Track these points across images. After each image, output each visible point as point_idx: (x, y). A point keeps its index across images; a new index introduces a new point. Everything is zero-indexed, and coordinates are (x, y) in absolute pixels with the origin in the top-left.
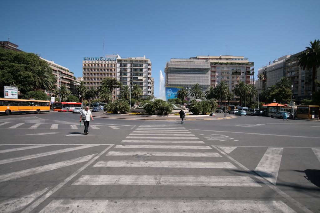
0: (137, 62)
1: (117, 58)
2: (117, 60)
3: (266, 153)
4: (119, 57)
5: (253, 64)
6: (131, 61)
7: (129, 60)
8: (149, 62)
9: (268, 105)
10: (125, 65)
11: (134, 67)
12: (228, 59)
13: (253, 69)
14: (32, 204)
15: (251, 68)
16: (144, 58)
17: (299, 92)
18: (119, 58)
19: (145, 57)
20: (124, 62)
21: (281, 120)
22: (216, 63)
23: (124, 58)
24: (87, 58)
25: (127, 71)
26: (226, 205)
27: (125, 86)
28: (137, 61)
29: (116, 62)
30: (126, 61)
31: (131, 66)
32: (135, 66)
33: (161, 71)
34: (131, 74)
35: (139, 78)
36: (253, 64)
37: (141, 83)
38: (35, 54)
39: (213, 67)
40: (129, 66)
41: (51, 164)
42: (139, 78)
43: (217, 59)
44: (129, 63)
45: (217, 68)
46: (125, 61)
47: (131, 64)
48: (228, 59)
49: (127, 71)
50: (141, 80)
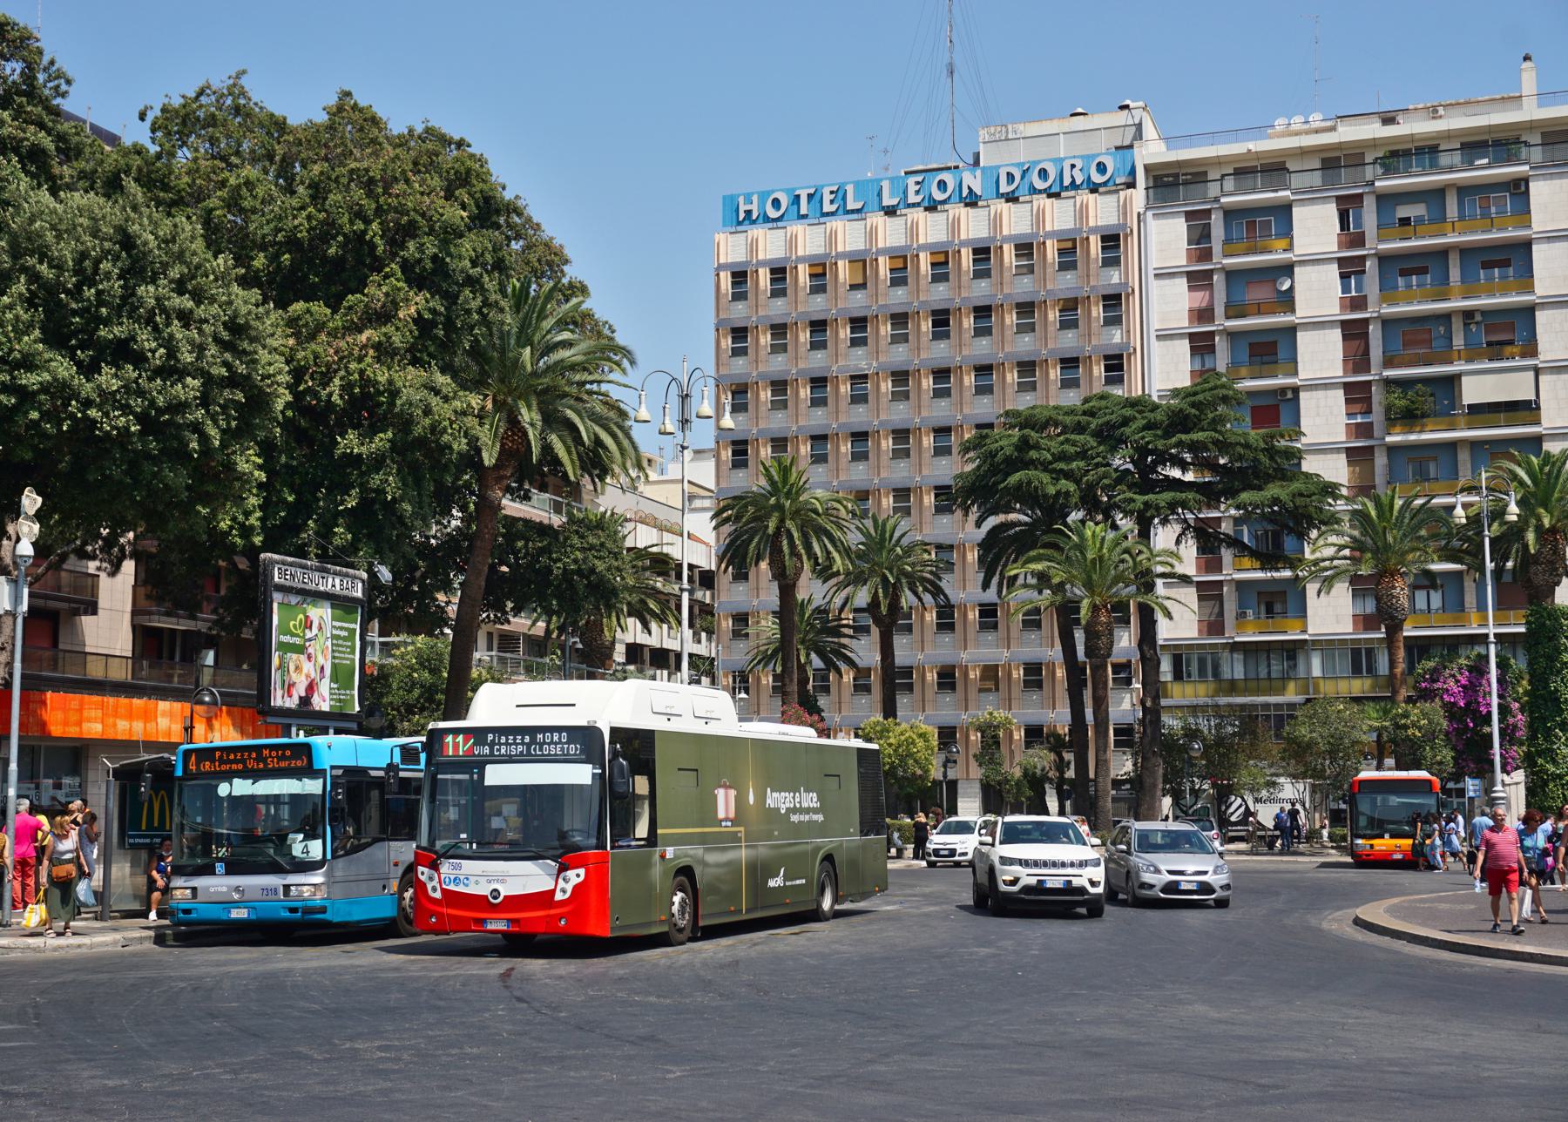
0: (1434, 167)
6: (1334, 161)
7: (1303, 152)
11: (1388, 363)
14: (1389, 651)
17: (63, 574)
21: (941, 540)
23: (1235, 134)
25: (1287, 301)
26: (935, 166)
29: (1138, 197)
30: (1273, 169)
31: (1352, 237)
32: (1410, 417)
34: (1354, 333)
38: (557, 242)
44: (1312, 196)
46: (1246, 171)
47: (1347, 208)
49: (1291, 308)
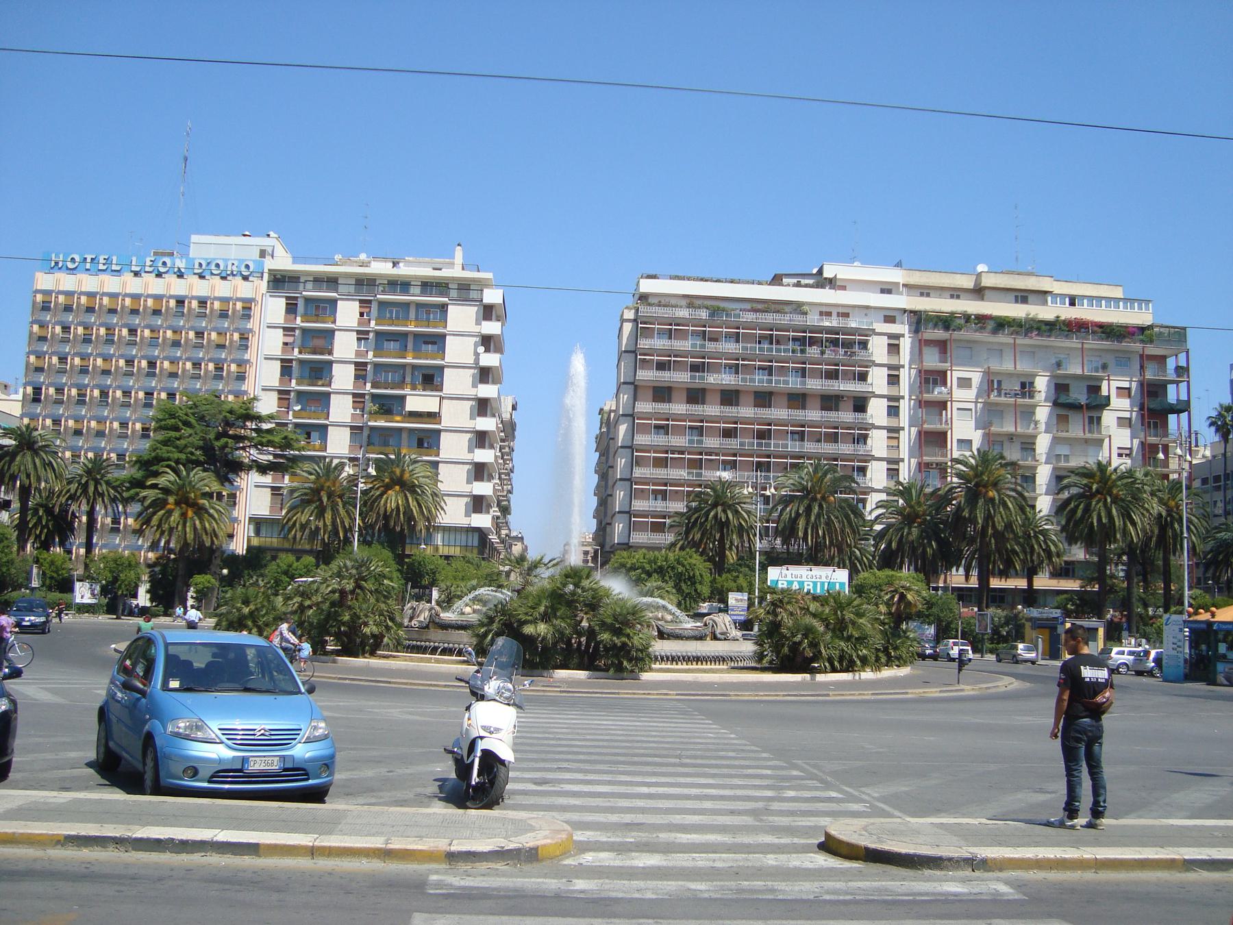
1: (269, 264)
2: (266, 276)
3: (14, 772)
4: (280, 251)
5: (1178, 336)
6: (365, 283)
7: (347, 275)
8: (492, 296)
9: (1213, 615)
10: (326, 308)
12: (1022, 296)
13: (1182, 371)
15: (1171, 363)
16: (455, 271)
18: (283, 261)
19: (459, 254)
20: (423, 293)
22: (946, 322)
24: (241, 261)
27: (1185, 535)
28: (402, 285)
30: (331, 281)
33: (578, 364)
35: (417, 401)
36: (1178, 336)
37: (427, 440)
39: (929, 343)
40: (348, 313)
41: (1020, 921)
42: (417, 401)
43: (955, 293)
45: (953, 350)
48: (1022, 296)
50: (433, 416)
